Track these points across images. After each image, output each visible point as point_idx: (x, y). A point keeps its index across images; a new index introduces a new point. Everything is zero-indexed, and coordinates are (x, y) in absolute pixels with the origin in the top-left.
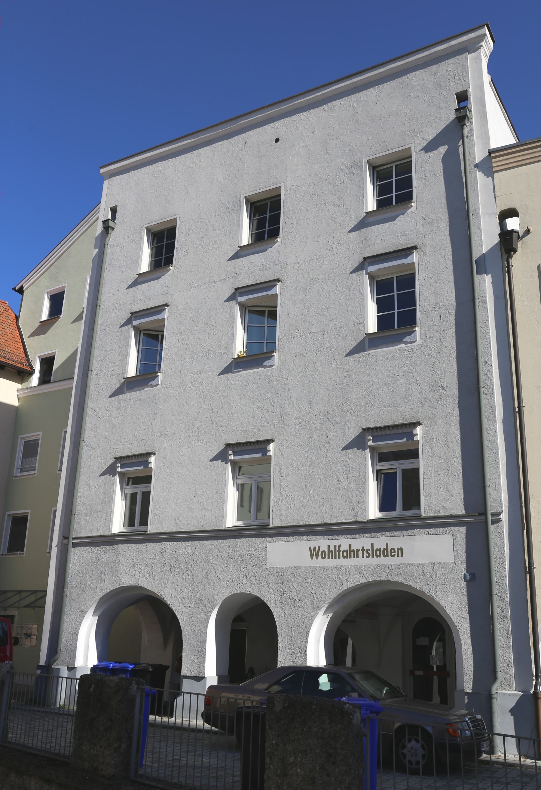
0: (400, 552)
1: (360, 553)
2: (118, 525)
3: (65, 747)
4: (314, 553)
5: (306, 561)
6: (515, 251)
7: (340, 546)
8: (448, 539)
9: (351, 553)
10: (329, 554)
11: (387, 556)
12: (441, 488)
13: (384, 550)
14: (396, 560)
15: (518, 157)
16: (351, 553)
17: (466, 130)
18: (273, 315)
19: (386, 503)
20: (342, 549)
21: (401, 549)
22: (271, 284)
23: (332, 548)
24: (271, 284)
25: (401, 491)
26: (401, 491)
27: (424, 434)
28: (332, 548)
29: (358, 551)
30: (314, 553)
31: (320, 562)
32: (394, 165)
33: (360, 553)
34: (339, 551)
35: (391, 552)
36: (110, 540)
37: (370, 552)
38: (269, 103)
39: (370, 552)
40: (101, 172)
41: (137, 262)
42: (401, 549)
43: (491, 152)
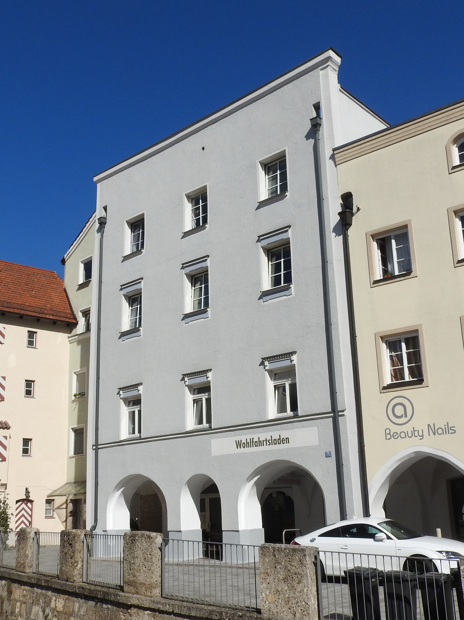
0: (287, 440)
1: (265, 442)
2: (124, 434)
3: (110, 576)
4: (239, 444)
5: (233, 449)
6: (350, 225)
7: (253, 439)
8: (315, 429)
9: (260, 443)
10: (247, 444)
11: (280, 443)
12: (312, 397)
13: (278, 439)
14: (285, 446)
15: (381, 140)
16: (260, 443)
17: (317, 135)
18: (287, 254)
19: (282, 408)
20: (254, 441)
21: (288, 438)
22: (204, 259)
23: (248, 441)
24: (204, 259)
25: (290, 400)
26: (290, 400)
27: (299, 360)
28: (248, 441)
29: (263, 441)
30: (239, 444)
31: (242, 450)
32: (278, 162)
33: (265, 442)
34: (253, 442)
35: (282, 441)
36: (120, 443)
37: (270, 441)
38: (338, 52)
39: (270, 441)
40: (94, 180)
41: (122, 247)
42: (288, 438)
43: (334, 150)
